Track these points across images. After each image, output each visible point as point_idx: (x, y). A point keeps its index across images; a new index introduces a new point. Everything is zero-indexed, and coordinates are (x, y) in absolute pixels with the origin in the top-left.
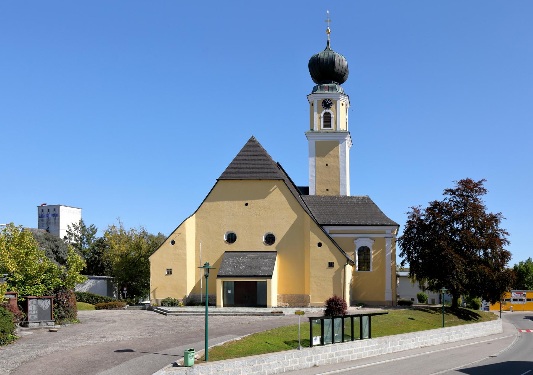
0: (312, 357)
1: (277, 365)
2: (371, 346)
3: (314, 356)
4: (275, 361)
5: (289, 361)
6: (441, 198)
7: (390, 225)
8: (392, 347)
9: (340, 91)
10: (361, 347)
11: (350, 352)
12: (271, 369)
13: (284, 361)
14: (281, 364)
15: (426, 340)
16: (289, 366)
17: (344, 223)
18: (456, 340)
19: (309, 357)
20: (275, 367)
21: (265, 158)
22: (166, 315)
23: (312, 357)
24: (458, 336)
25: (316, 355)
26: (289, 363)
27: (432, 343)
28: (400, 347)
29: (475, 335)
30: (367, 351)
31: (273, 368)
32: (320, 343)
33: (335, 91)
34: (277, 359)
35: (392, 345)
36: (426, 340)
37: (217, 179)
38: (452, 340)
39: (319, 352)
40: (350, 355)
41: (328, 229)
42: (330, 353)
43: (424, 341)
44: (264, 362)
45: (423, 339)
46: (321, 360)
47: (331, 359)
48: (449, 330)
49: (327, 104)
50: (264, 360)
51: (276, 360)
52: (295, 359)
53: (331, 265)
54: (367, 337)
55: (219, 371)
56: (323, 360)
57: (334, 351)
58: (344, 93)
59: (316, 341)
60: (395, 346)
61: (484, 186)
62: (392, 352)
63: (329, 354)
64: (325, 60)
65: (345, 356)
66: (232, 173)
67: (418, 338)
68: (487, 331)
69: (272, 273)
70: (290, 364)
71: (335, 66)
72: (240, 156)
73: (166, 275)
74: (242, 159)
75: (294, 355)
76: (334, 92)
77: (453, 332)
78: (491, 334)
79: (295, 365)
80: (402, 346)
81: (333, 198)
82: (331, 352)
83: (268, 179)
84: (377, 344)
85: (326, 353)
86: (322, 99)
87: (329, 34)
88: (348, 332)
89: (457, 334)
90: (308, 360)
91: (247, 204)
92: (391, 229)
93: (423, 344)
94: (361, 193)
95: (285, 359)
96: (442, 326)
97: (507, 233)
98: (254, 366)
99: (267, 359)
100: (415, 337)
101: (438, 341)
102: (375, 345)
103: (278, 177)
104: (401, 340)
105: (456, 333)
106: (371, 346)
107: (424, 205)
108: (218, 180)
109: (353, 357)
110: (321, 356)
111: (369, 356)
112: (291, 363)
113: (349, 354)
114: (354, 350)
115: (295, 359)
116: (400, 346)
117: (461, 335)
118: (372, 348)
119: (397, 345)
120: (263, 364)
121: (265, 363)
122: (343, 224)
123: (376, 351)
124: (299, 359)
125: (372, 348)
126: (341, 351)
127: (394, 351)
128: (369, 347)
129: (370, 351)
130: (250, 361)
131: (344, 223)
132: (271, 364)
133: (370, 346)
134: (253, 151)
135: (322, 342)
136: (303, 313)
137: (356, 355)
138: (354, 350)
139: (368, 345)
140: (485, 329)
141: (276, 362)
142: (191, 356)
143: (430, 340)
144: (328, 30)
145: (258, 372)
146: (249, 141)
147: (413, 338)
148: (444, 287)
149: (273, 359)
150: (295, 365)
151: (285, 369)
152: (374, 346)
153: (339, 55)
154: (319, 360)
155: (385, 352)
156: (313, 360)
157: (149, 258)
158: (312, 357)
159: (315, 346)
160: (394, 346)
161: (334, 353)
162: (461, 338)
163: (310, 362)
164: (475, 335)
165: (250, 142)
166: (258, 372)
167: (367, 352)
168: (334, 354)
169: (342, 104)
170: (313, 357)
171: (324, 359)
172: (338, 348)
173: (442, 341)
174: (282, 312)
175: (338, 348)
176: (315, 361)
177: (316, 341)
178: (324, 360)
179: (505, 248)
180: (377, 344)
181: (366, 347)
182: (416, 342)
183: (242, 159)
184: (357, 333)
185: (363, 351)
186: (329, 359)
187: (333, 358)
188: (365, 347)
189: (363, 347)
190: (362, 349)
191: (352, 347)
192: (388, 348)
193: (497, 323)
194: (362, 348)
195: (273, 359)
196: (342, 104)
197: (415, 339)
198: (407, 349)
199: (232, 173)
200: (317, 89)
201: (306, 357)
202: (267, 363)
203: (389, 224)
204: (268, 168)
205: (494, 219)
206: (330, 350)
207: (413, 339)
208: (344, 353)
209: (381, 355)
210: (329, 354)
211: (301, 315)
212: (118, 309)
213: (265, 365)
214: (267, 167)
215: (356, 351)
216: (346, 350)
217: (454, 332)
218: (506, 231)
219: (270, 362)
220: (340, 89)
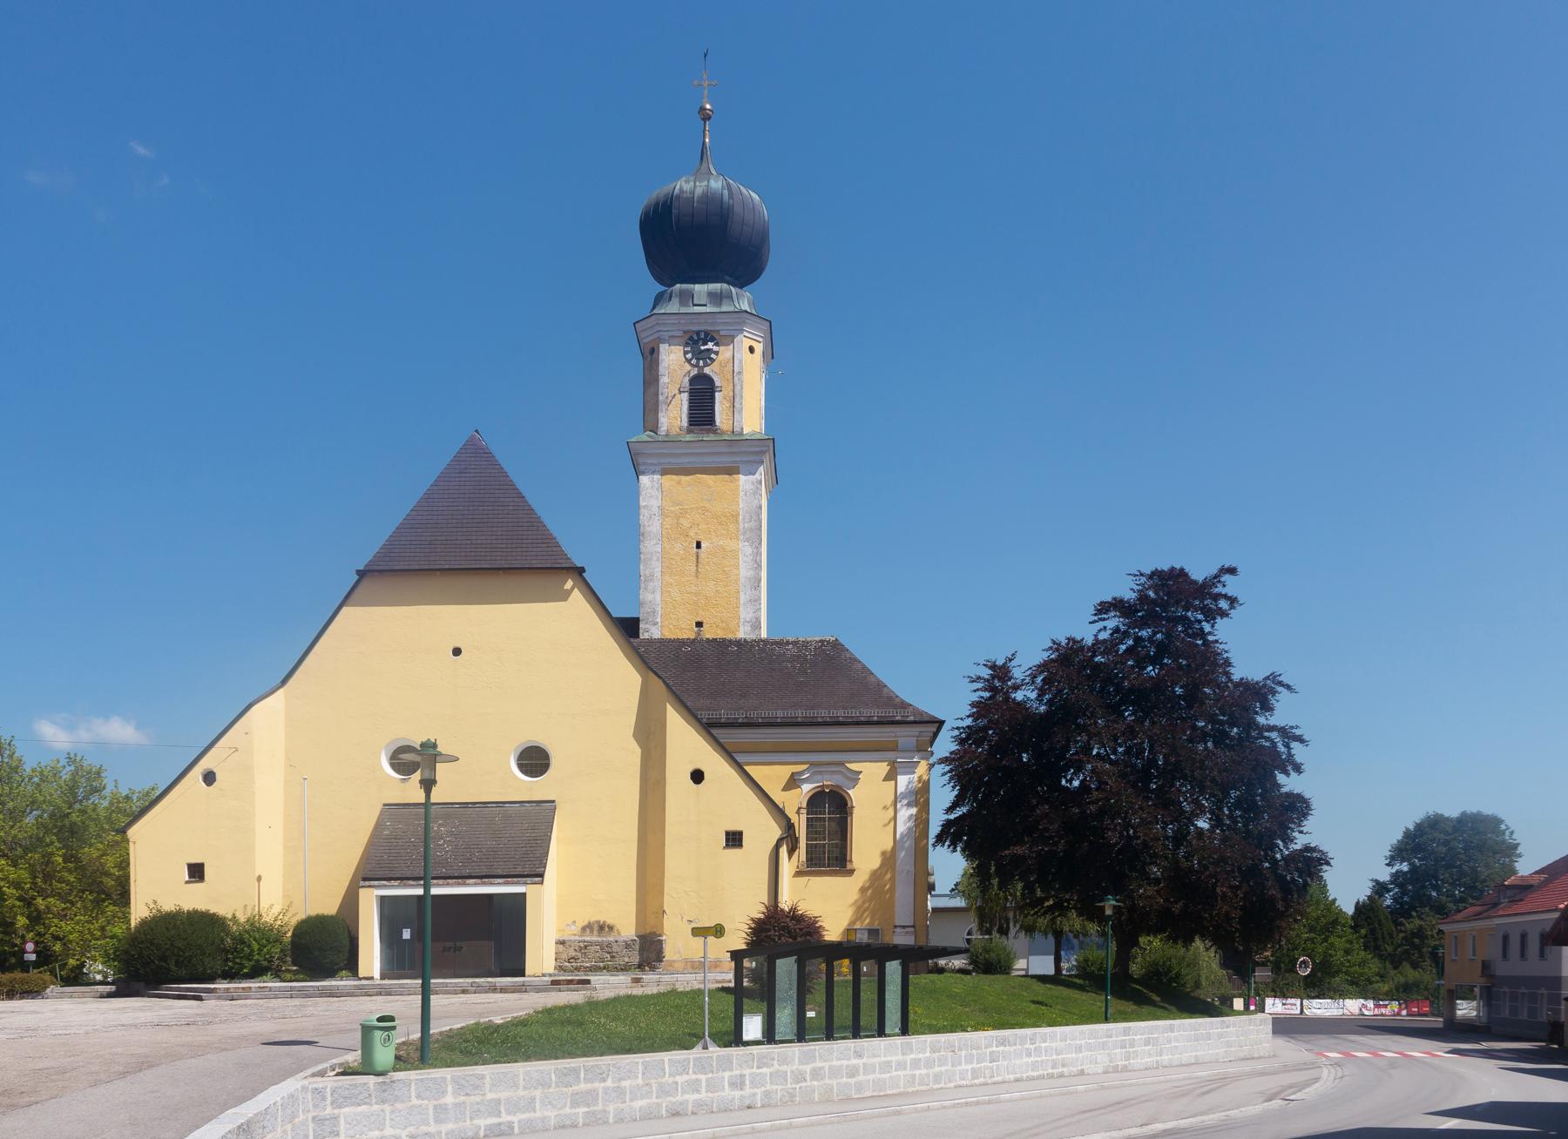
0: (742, 1076)
1: (644, 1092)
2: (912, 1056)
3: (750, 1074)
4: (637, 1077)
5: (677, 1083)
6: (1087, 633)
7: (915, 722)
8: (969, 1067)
9: (745, 306)
10: (883, 1059)
11: (853, 1072)
12: (625, 1102)
13: (663, 1080)
14: (654, 1089)
15: (1063, 1056)
16: (678, 1098)
17: (762, 718)
18: (1147, 1062)
19: (736, 1076)
20: (637, 1099)
21: (516, 500)
22: (199, 999)
23: (745, 1075)
24: (1151, 1052)
25: (755, 1070)
26: (677, 1090)
27: (1079, 1068)
28: (992, 1068)
29: (1198, 1053)
30: (901, 1073)
31: (631, 1100)
32: (763, 1037)
33: (730, 305)
34: (643, 1074)
35: (969, 1059)
36: (1063, 1056)
37: (358, 572)
38: (1136, 1062)
39: (765, 1061)
40: (852, 1081)
41: (714, 731)
42: (794, 1068)
43: (1059, 1057)
44: (604, 1080)
45: (1056, 1050)
46: (769, 1087)
47: (798, 1086)
48: (1126, 1032)
49: (699, 342)
50: (604, 1073)
51: (640, 1075)
52: (694, 1077)
53: (734, 840)
54: (897, 1030)
55: (470, 1095)
56: (775, 1087)
57: (807, 1064)
58: (754, 312)
59: (753, 1026)
60: (979, 1065)
61: (1231, 586)
62: (968, 1083)
63: (792, 1072)
64: (695, 205)
65: (838, 1084)
66: (408, 551)
67: (1043, 1045)
68: (1231, 1047)
69: (545, 867)
70: (680, 1094)
71: (729, 224)
72: (437, 496)
73: (187, 882)
74: (440, 504)
75: (691, 1064)
76: (725, 308)
77: (1139, 1037)
78: (1242, 1055)
79: (696, 1096)
80: (998, 1067)
81: (721, 647)
82: (799, 1065)
83: (529, 568)
84: (928, 1054)
85: (784, 1068)
86: (685, 332)
87: (707, 123)
88: (843, 1013)
89: (1151, 1047)
90: (733, 1085)
91: (197, 872)
92: (917, 734)
93: (1056, 1068)
94: (811, 631)
95: (667, 1075)
96: (1104, 1018)
97: (1300, 739)
98: (576, 1088)
99: (614, 1070)
100: (1033, 1041)
101: (1096, 1063)
102: (921, 1056)
103: (561, 561)
104: (994, 1049)
105: (1147, 1042)
106: (912, 1056)
107: (1029, 655)
108: (362, 574)
109: (860, 1087)
110: (771, 1074)
111: (904, 1087)
112: (682, 1088)
113: (850, 1078)
114: (864, 1064)
115: (694, 1077)
116: (991, 1065)
117: (1161, 1049)
118: (916, 1064)
119: (985, 1061)
120: (602, 1084)
121: (609, 1083)
122: (760, 720)
123: (926, 1074)
124: (707, 1080)
125: (916, 1064)
126: (826, 1065)
127: (976, 1081)
128: (905, 1062)
129: (908, 1072)
130: (565, 1071)
131: (762, 718)
132: (625, 1087)
133: (909, 1058)
134: (478, 479)
135: (770, 1036)
136: (720, 931)
137: (869, 1080)
138: (864, 1064)
139: (903, 1054)
140: (1225, 1040)
141: (640, 1081)
142: (385, 1039)
143: (1074, 1055)
144: (703, 109)
145: (586, 1109)
146: (464, 448)
147: (1027, 1046)
148: (1110, 897)
149: (630, 1071)
150: (696, 1096)
151: (667, 1106)
152: (920, 1059)
153: (741, 187)
154: (763, 1089)
155: (950, 1081)
156: (748, 1087)
157: (131, 833)
158: (745, 1075)
159: (748, 1043)
160: (974, 1065)
161: (808, 1068)
162: (1159, 1058)
163: (737, 1093)
164: (1198, 1053)
165: (468, 451)
166: (586, 1109)
167: (899, 1076)
168: (806, 1072)
169: (751, 350)
170: (747, 1077)
171: (777, 1084)
172: (820, 1054)
173: (1108, 1064)
174: (588, 982)
175: (817, 1054)
176: (751, 1090)
177: (753, 1026)
178: (777, 1090)
179: (1289, 783)
180: (928, 1054)
181: (897, 1058)
182: (1037, 1059)
183: (440, 504)
184: (868, 1017)
185: (889, 1072)
186: (794, 1086)
187: (804, 1084)
188: (894, 1058)
189: (889, 1058)
190: (886, 1067)
191: (859, 1055)
192: (960, 1068)
193: (1258, 1023)
194: (885, 1062)
195: (630, 1071)
196: (751, 350)
197: (1032, 1047)
198: (1012, 1077)
199: (408, 551)
200: (670, 299)
201: (727, 1075)
202: (613, 1082)
203: (912, 718)
204: (530, 533)
205: (1260, 694)
206: (797, 1060)
207: (1027, 1049)
208: (835, 1072)
209: (941, 1088)
210: (792, 1072)
211: (711, 939)
212: (21, 999)
213: (608, 1088)
214: (525, 528)
215: (868, 1069)
216: (839, 1063)
217: (1140, 1039)
218: (1297, 732)
219: (625, 1079)
220: (744, 300)
